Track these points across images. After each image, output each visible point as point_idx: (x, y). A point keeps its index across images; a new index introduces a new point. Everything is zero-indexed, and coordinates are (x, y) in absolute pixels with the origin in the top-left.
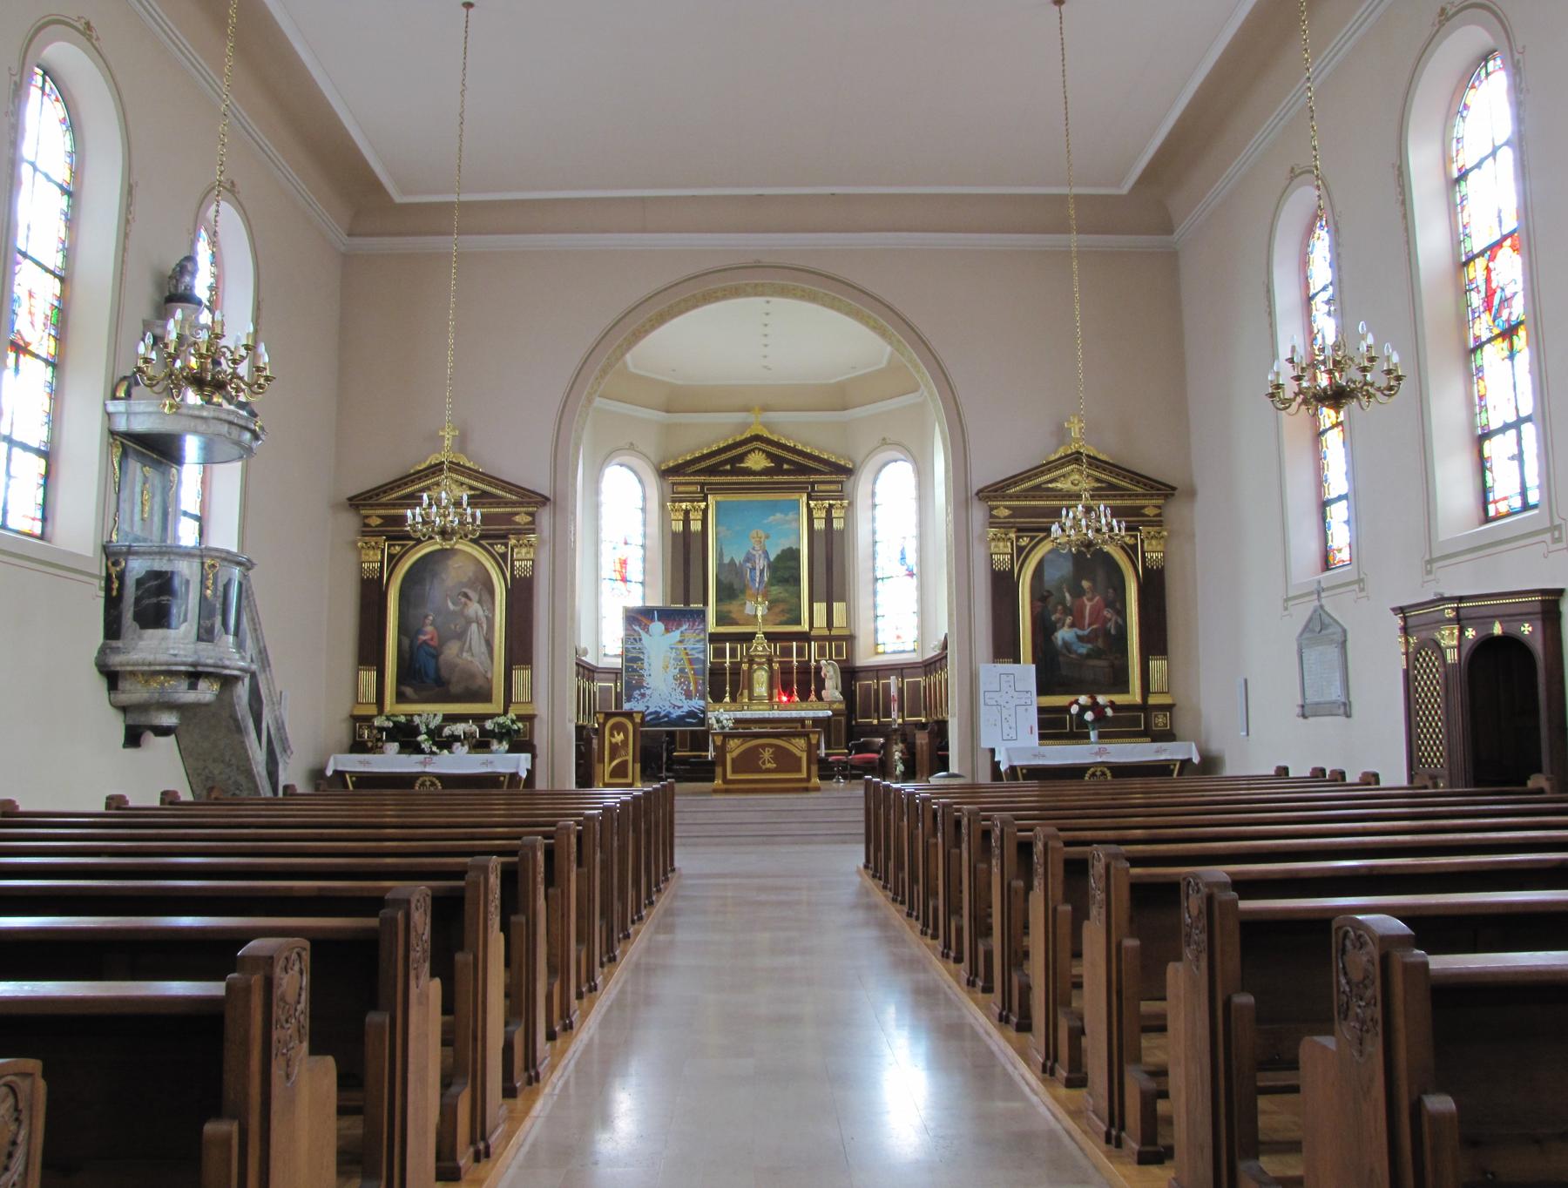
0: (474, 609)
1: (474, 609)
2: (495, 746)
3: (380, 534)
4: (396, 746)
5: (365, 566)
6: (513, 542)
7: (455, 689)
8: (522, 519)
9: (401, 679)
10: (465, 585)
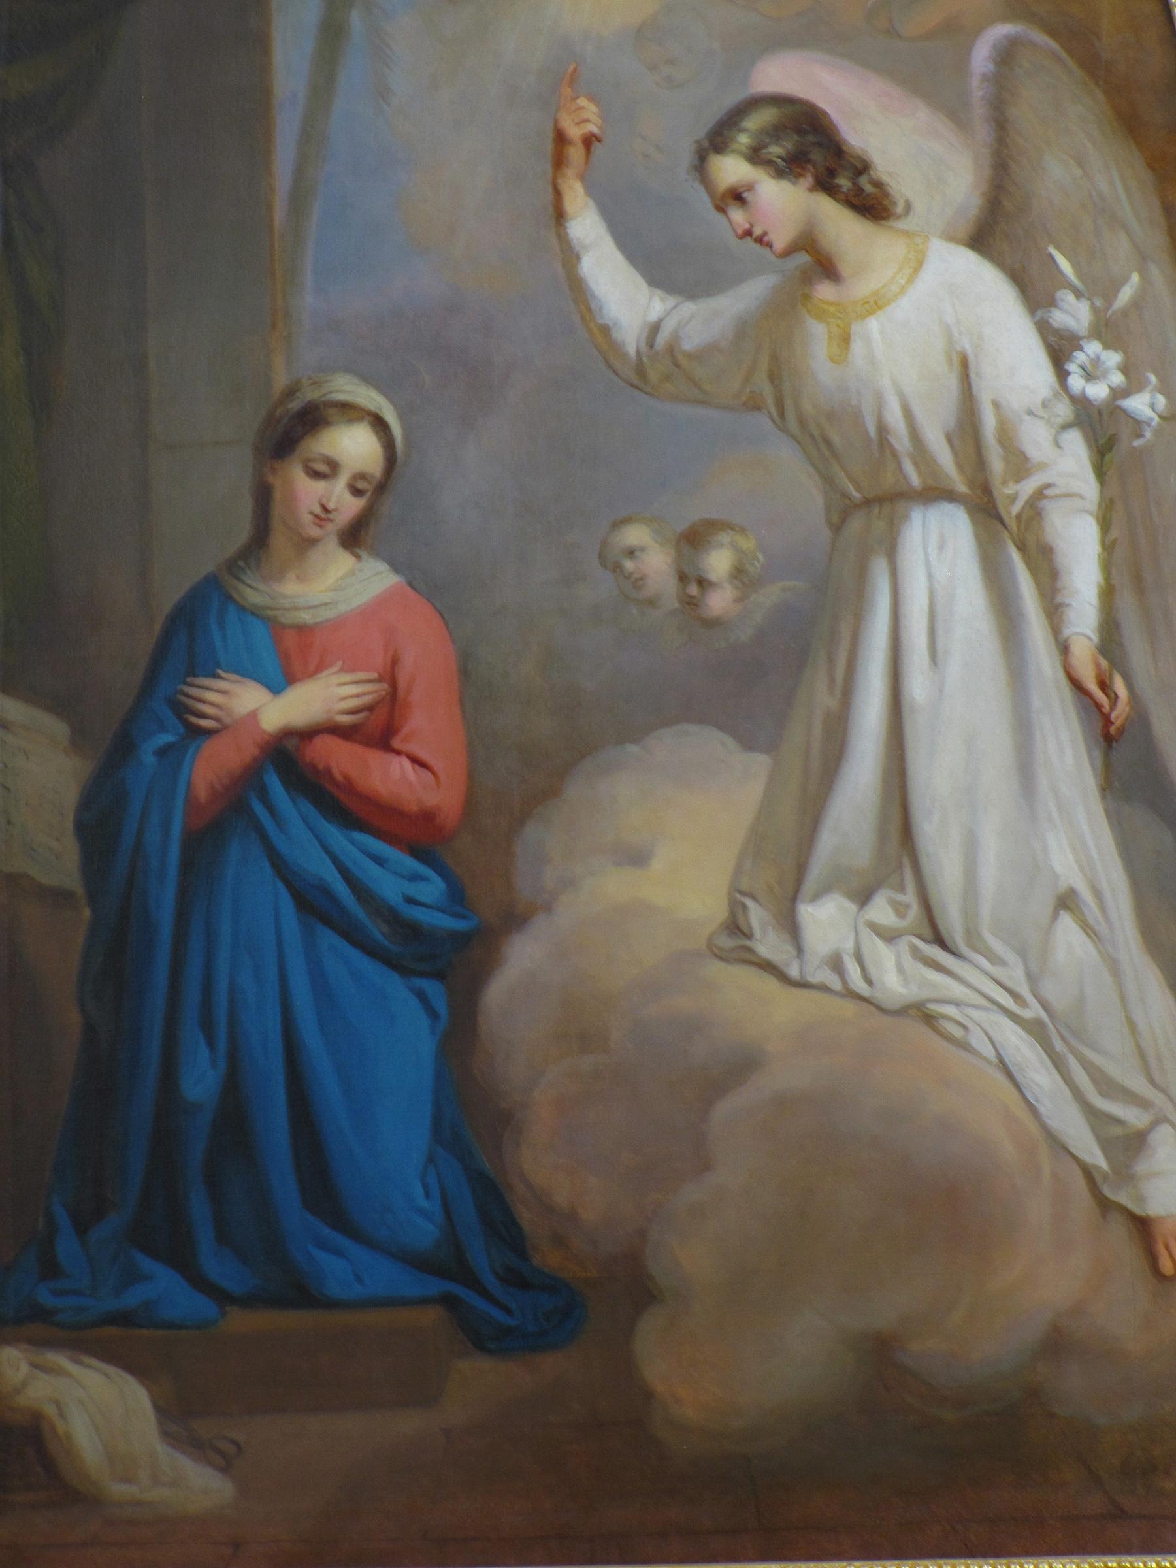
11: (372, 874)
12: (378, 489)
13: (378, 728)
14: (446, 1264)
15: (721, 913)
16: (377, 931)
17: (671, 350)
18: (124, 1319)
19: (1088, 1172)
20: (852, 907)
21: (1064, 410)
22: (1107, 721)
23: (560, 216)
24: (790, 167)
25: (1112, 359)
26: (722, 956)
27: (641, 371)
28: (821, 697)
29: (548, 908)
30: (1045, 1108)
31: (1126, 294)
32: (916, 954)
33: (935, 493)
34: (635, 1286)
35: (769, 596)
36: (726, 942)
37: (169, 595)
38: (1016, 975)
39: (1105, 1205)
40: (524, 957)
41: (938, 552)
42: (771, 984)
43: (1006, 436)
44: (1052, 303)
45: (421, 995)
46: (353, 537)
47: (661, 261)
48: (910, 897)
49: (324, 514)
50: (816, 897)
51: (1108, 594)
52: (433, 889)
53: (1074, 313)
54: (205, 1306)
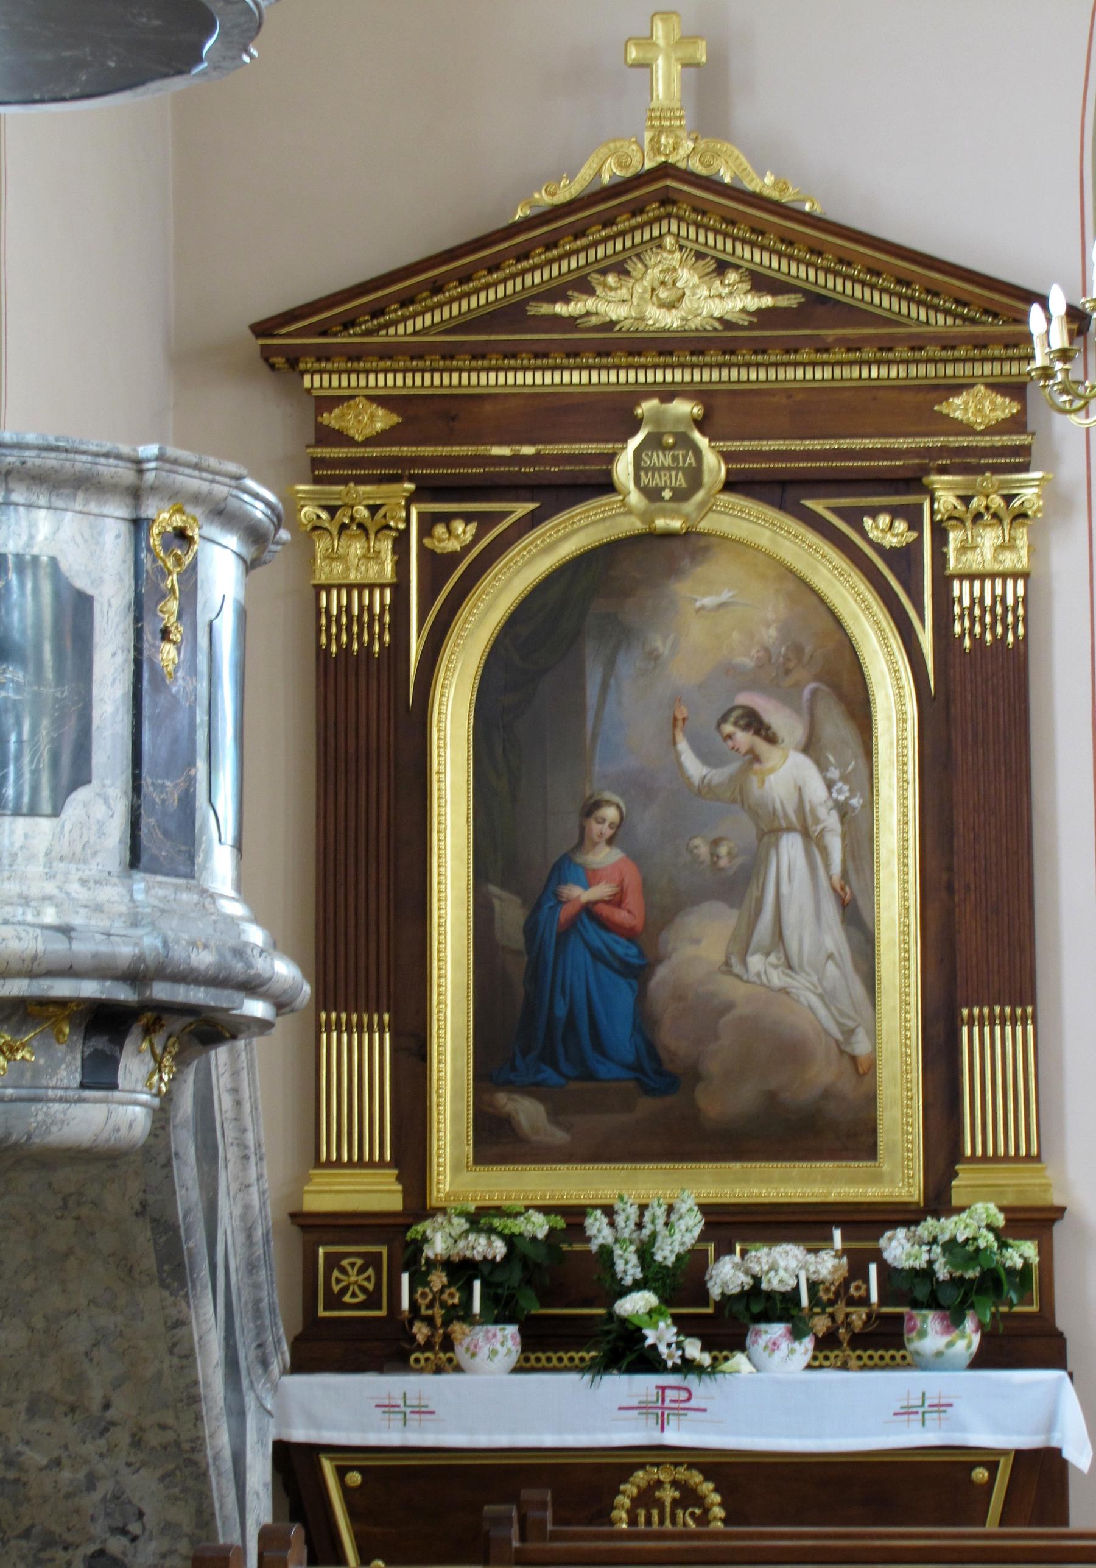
0: (790, 775)
1: (790, 775)
2: (931, 1335)
3: (387, 472)
4: (506, 1339)
5: (334, 601)
6: (946, 493)
7: (722, 1101)
8: (976, 408)
9: (497, 1061)
10: (752, 682)
11: (614, 946)
12: (619, 826)
13: (617, 901)
14: (636, 1068)
15: (723, 959)
16: (616, 964)
17: (709, 784)
18: (537, 1084)
19: (837, 1042)
20: (763, 958)
21: (831, 804)
22: (843, 901)
23: (674, 743)
24: (746, 727)
25: (846, 788)
26: (724, 973)
27: (699, 791)
28: (754, 892)
29: (670, 957)
30: (823, 1021)
31: (850, 768)
32: (783, 972)
33: (790, 829)
34: (695, 1075)
35: (738, 861)
36: (724, 968)
37: (553, 859)
38: (815, 979)
39: (842, 1052)
40: (661, 973)
41: (791, 847)
42: (739, 982)
43: (813, 811)
44: (827, 770)
45: (629, 984)
46: (610, 841)
47: (705, 756)
48: (782, 954)
49: (601, 835)
50: (752, 955)
51: (844, 861)
52: (633, 951)
53: (834, 773)
54: (562, 1081)
